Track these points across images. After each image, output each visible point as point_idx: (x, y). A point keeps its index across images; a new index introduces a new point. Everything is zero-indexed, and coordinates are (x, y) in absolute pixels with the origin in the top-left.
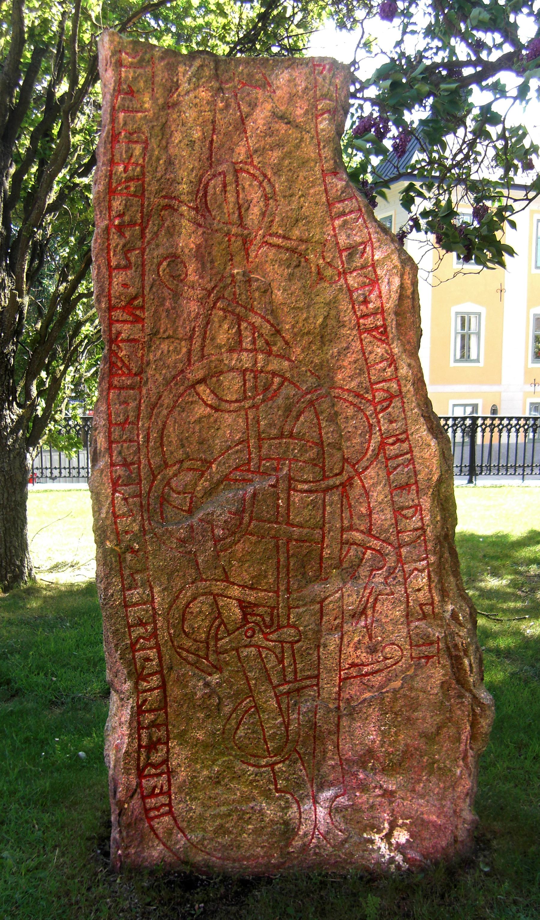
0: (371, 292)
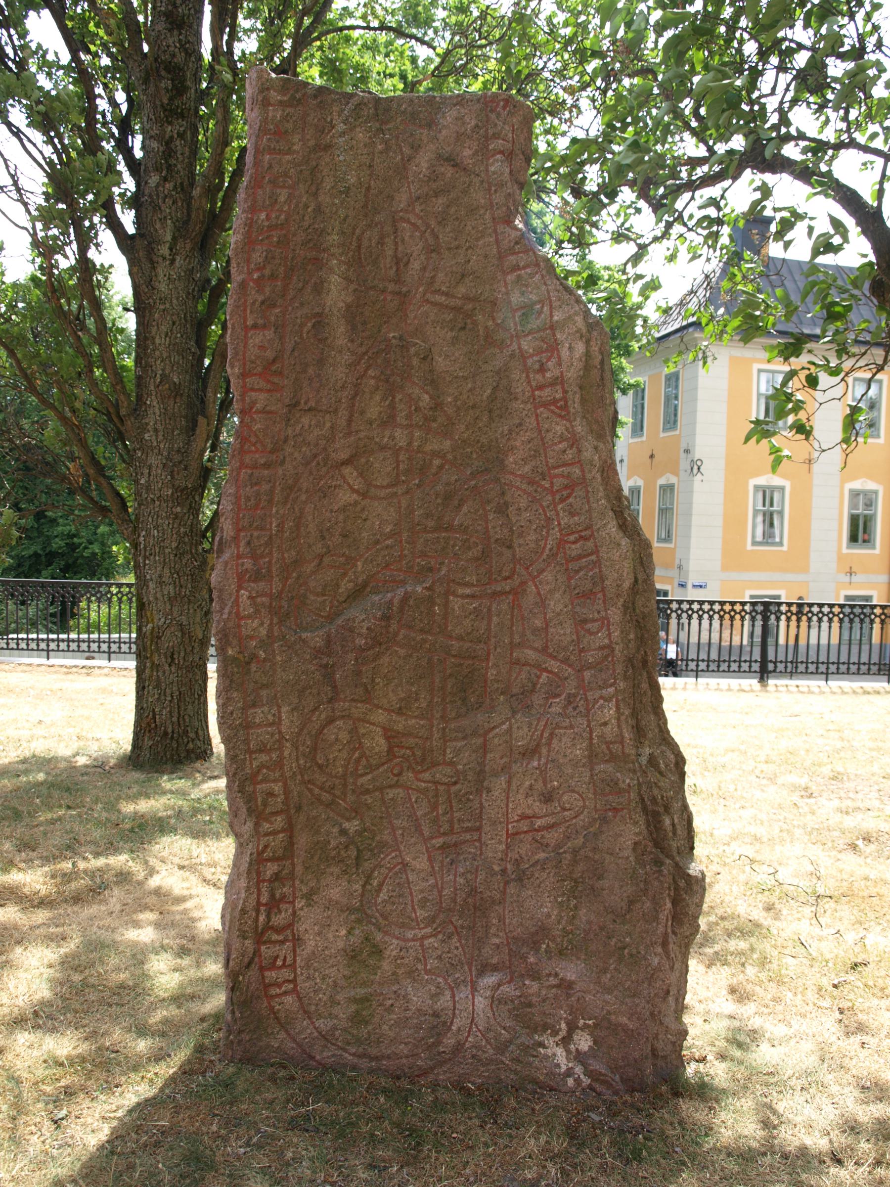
0: (549, 360)
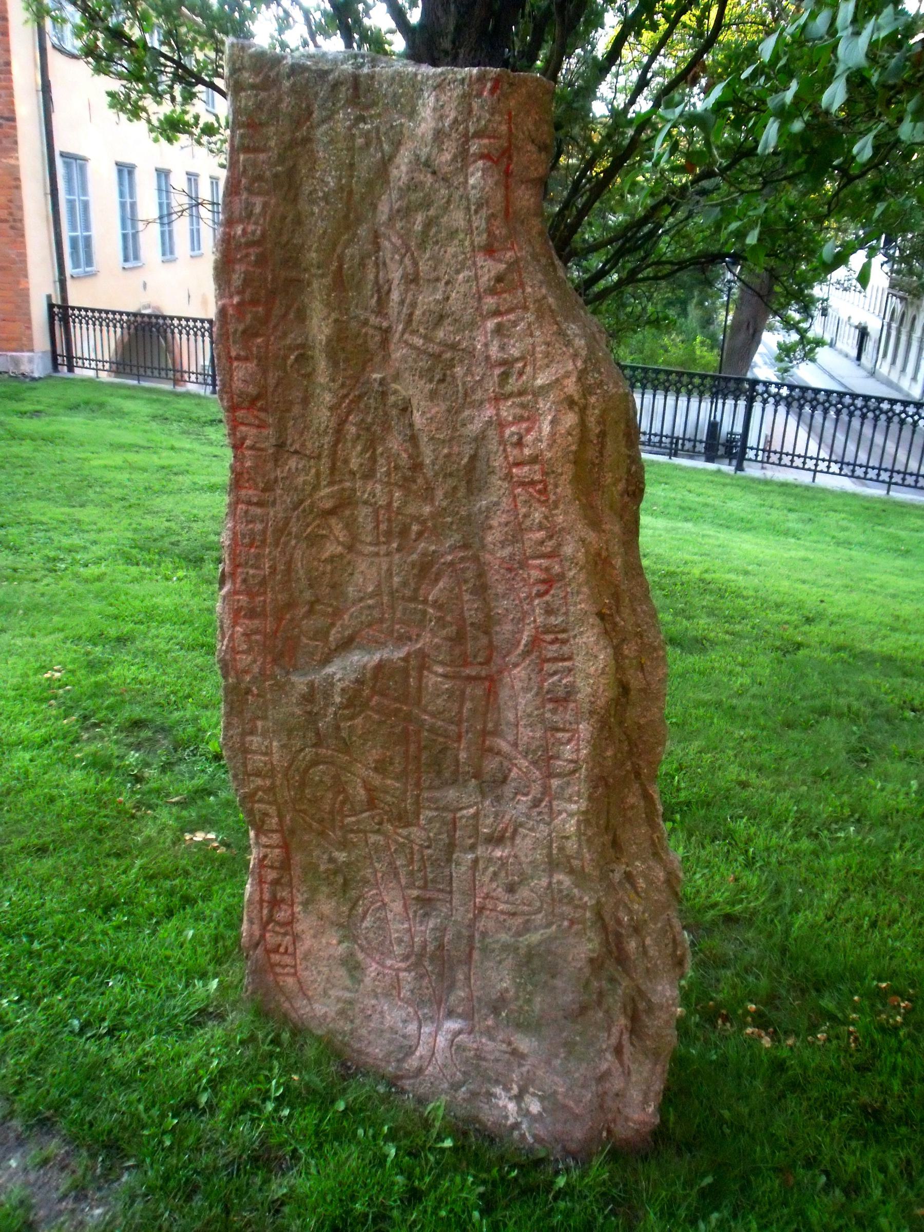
0: (528, 430)
